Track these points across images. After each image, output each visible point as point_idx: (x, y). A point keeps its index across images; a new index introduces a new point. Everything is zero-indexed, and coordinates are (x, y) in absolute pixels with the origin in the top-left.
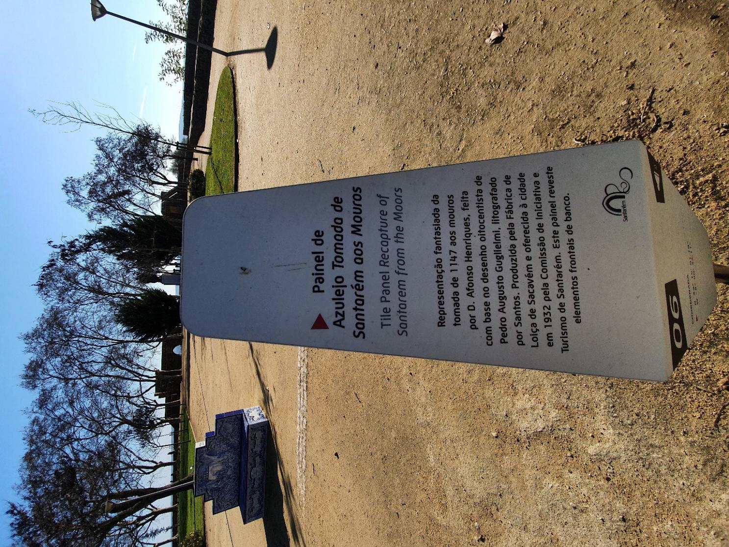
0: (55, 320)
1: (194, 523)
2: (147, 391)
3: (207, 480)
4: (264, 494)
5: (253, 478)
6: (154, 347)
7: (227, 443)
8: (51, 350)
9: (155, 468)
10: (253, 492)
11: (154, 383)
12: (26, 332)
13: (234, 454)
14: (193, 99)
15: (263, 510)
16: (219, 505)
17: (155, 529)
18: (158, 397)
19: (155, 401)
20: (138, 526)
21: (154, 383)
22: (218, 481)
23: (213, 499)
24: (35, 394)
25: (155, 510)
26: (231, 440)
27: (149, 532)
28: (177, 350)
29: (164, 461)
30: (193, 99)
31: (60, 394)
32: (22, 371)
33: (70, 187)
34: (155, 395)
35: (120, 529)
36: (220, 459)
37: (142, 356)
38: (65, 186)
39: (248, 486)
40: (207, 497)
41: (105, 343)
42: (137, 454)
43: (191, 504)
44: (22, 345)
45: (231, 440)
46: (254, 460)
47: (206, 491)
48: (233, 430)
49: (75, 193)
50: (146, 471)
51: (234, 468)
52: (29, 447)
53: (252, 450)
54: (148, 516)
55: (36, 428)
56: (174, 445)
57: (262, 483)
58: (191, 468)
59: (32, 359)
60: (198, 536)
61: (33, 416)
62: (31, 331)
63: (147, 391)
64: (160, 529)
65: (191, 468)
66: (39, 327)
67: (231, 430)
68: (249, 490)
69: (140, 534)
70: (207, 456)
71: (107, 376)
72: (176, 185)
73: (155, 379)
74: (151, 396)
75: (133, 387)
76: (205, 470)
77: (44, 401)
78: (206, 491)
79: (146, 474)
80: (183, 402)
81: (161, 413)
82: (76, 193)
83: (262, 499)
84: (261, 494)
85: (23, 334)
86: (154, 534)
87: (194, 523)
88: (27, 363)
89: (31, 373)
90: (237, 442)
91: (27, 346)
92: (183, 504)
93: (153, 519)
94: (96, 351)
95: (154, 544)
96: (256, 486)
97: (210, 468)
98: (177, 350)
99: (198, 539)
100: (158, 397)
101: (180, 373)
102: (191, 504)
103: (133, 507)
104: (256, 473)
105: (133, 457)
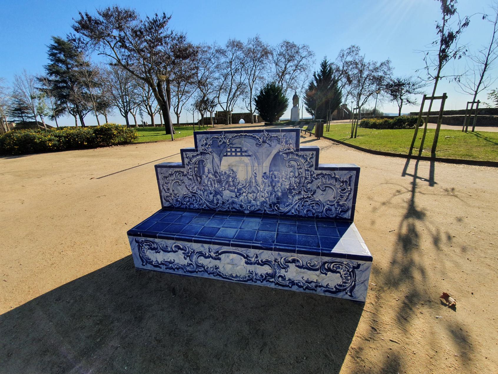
0: (266, 53)
1: (144, 136)
2: (221, 106)
3: (222, 154)
4: (180, 272)
5: (222, 256)
6: (247, 108)
7: (290, 190)
8: (249, 52)
9: (177, 114)
10: (188, 255)
11: (225, 109)
12: (260, 37)
13: (263, 203)
14: (487, 116)
15: (149, 267)
16: (171, 175)
17: (143, 114)
18: (216, 113)
19: (214, 111)
20: (146, 106)
21: (225, 109)
22: (215, 173)
23: (183, 166)
24: (224, 47)
25: (153, 115)
26: (297, 198)
27: (142, 111)
28: (242, 121)
29: (180, 118)
30: (487, 116)
31: (223, 60)
32: (238, 39)
33: (353, 50)
34: (216, 111)
35: (146, 97)
36: (260, 179)
37: (243, 101)
38: (353, 47)
39: (206, 246)
40: (190, 154)
41: (251, 81)
42: (186, 103)
43: (155, 134)
44: (253, 36)
45: (297, 198)
46: (263, 263)
47: (202, 153)
48: (318, 203)
49: (349, 53)
50: (176, 110)
51: (233, 203)
52: (196, 46)
53: (294, 261)
54: (151, 111)
55: (205, 49)
56: (188, 123)
57: (206, 271)
58: (179, 132)
59: (243, 44)
60: (134, 139)
61: (212, 47)
62: (260, 40)
63: (221, 106)
64: (143, 117)
65: (179, 132)
66: (263, 44)
67: (319, 197)
68: (197, 247)
69: (142, 107)
70: (274, 152)
71: (232, 84)
72: (353, 112)
73: (228, 110)
74: (218, 109)
75: (223, 98)
76: (245, 149)
77: (220, 52)
78: (202, 153)
79: (174, 109)
80: (215, 126)
81: (207, 115)
82: (349, 53)
83: (171, 268)
84: (183, 267)
85: (259, 36)
86: (141, 114)
87: (144, 136)
88: (242, 41)
89: (236, 44)
90: (286, 209)
91: (252, 39)
92: (155, 129)
93: (149, 114)
94: (247, 76)
95: (135, 115)
96: (202, 260)
97: (246, 159)
98: (242, 121)
99: (132, 138)
100: (216, 113)
101: (230, 123)
102: (155, 134)
103: (160, 97)
104: (232, 263)
105: (185, 101)
